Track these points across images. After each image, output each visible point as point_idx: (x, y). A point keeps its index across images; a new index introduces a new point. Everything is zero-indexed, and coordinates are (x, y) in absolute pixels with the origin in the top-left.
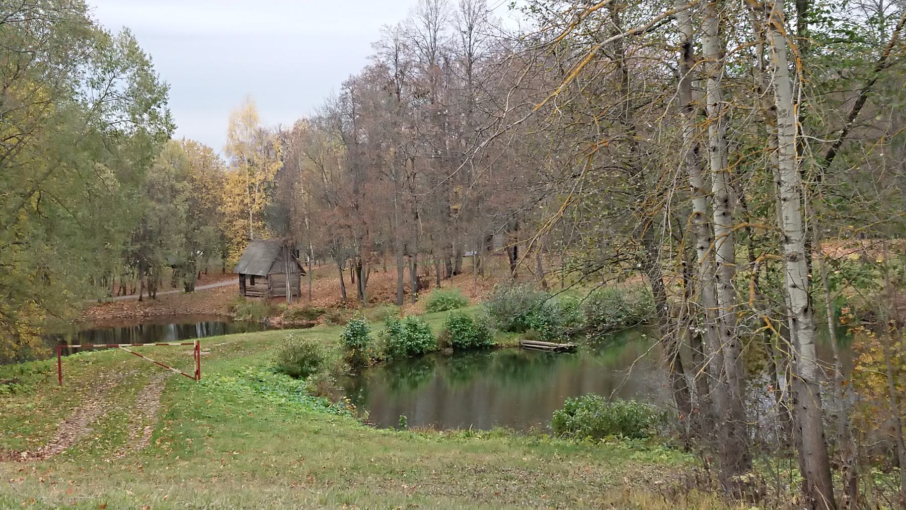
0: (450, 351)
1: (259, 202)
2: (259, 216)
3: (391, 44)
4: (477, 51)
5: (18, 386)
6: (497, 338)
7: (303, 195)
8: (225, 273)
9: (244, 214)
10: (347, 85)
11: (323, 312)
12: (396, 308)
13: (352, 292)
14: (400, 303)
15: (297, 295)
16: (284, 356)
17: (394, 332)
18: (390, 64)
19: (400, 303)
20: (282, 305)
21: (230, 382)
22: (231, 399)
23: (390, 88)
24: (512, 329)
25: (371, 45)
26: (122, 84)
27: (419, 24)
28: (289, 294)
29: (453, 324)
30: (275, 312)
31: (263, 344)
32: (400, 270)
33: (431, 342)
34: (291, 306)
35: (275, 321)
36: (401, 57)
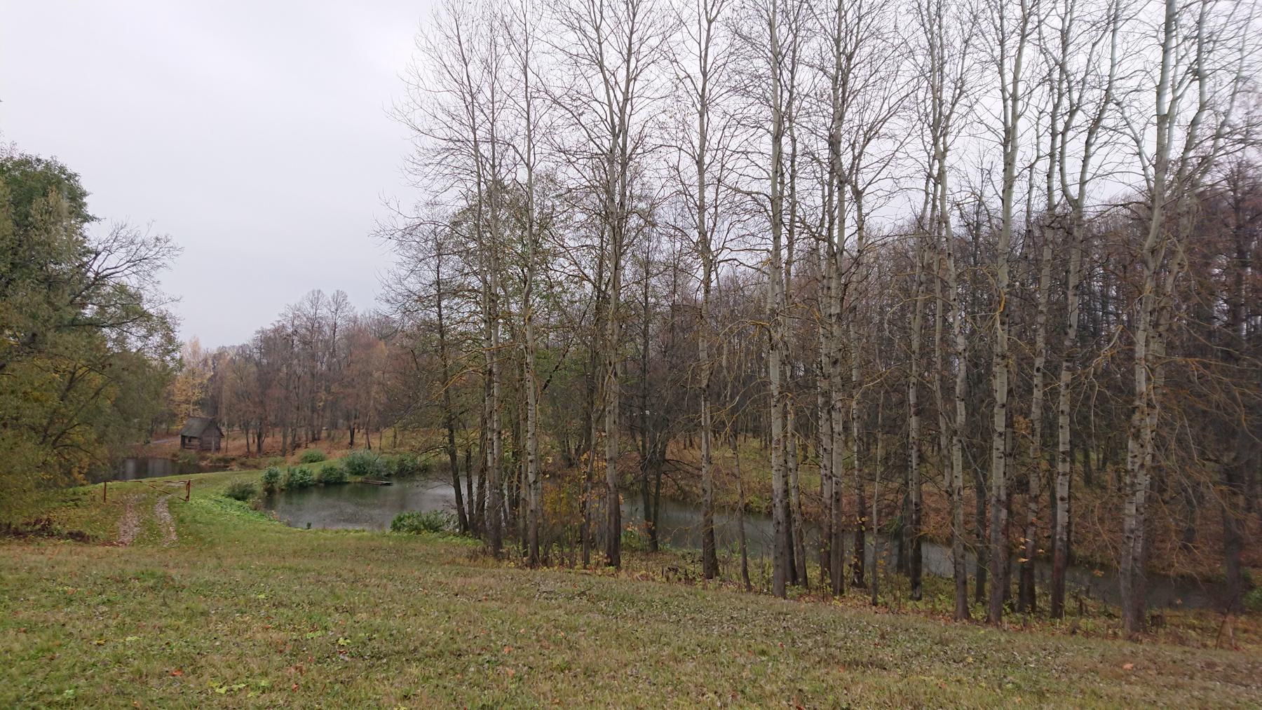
0: (322, 485)
1: (198, 395)
2: (196, 403)
3: (291, 315)
4: (339, 323)
5: (79, 503)
6: (349, 478)
7: (226, 395)
8: (168, 434)
9: (187, 402)
10: (258, 332)
11: (233, 459)
12: (282, 459)
13: (254, 448)
14: (284, 455)
15: (218, 449)
16: (233, 489)
17: (292, 475)
18: (289, 325)
19: (284, 455)
20: (209, 455)
21: (205, 502)
22: (209, 512)
23: (287, 340)
24: (358, 474)
25: (162, 235)
26: (156, 339)
27: (307, 305)
28: (213, 448)
29: (325, 471)
30: (204, 458)
31: (216, 482)
32: (285, 437)
33: (313, 480)
34: (213, 455)
35: (203, 463)
36: (296, 322)
